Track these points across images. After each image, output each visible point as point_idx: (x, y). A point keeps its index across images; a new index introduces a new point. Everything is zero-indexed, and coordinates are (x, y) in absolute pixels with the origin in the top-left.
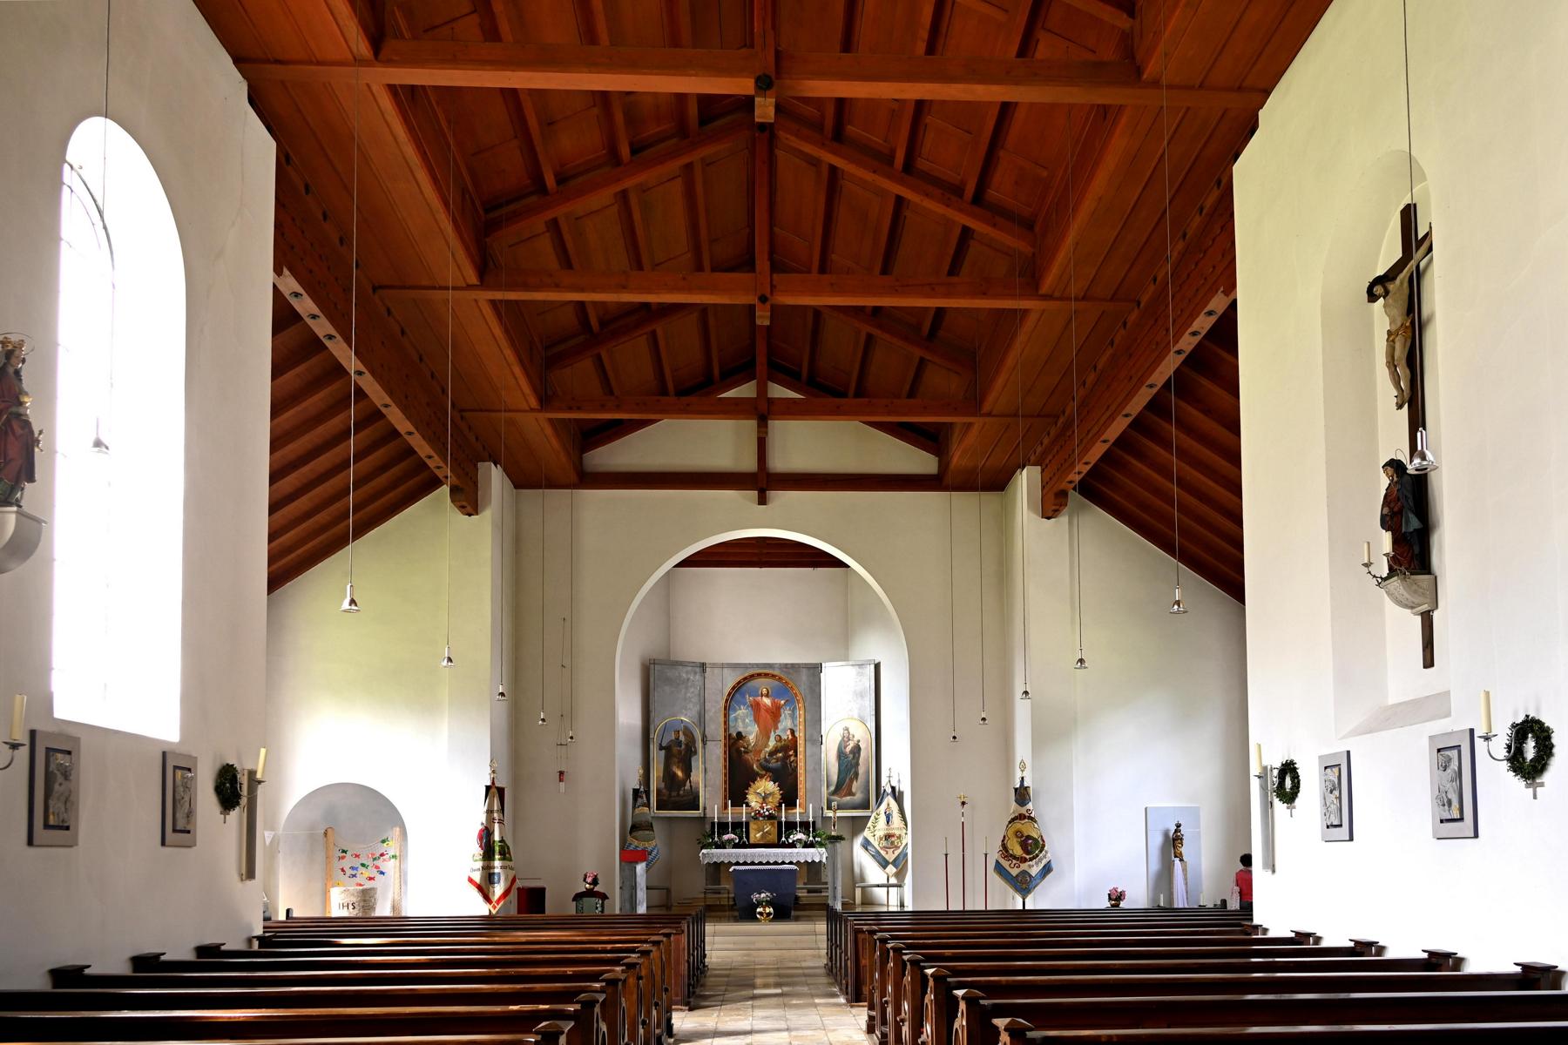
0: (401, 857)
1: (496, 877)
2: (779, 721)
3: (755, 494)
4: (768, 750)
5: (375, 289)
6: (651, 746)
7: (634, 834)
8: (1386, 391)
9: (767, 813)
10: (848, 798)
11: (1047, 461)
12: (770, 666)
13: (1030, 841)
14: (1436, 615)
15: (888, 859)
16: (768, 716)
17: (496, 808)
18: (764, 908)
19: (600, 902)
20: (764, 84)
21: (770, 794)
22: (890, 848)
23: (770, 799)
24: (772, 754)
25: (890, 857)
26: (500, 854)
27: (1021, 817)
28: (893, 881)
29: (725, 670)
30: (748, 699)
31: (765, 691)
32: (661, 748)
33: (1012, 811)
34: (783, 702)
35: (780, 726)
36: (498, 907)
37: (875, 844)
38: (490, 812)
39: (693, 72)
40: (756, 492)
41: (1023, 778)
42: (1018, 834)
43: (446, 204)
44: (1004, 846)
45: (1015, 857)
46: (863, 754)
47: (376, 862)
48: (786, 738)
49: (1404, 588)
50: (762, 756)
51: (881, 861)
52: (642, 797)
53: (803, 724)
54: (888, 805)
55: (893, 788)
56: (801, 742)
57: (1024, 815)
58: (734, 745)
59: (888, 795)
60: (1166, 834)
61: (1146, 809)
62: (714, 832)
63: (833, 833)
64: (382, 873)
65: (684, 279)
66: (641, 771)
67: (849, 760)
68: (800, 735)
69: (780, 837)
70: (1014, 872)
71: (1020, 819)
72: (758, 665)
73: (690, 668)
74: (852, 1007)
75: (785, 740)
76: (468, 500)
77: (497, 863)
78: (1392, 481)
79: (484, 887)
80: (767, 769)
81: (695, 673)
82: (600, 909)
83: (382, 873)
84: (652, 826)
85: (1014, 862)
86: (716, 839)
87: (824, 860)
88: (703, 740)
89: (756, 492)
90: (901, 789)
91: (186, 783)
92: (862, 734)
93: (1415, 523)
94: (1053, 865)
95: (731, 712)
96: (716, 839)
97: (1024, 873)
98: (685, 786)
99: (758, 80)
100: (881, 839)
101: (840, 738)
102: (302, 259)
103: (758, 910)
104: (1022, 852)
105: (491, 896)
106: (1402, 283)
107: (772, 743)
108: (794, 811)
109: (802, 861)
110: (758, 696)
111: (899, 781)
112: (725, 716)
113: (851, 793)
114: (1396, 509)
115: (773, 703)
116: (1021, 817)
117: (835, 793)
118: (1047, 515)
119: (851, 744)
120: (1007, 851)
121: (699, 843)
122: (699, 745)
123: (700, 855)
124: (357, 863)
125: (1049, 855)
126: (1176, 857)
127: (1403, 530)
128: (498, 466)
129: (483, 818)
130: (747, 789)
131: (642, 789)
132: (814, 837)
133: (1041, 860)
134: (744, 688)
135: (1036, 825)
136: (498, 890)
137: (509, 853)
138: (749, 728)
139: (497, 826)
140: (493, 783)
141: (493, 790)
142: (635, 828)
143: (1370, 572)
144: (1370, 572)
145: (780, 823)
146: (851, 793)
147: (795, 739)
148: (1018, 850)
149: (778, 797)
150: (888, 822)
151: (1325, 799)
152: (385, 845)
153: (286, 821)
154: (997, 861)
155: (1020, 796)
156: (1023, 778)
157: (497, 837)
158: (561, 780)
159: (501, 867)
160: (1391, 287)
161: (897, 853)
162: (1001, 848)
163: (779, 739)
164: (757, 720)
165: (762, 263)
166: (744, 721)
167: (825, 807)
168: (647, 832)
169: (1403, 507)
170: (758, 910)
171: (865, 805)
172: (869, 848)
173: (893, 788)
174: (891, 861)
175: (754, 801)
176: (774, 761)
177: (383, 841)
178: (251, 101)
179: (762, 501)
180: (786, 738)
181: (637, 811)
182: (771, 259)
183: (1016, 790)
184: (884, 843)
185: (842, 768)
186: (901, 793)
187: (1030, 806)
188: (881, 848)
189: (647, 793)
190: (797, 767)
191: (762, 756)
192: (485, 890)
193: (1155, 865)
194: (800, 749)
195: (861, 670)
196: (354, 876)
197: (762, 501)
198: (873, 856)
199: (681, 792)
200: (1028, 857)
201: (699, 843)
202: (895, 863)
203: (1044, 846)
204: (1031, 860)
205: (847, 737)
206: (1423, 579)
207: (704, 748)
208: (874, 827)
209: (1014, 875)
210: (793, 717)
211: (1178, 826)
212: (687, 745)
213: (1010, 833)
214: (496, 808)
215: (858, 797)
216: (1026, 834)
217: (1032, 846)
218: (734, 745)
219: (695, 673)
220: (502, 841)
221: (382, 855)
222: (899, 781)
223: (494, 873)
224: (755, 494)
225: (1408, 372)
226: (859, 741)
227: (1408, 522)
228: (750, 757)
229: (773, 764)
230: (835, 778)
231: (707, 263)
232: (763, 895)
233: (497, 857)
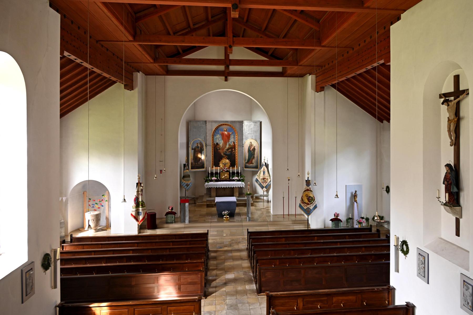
0: (109, 201)
1: (140, 213)
2: (230, 139)
3: (224, 77)
4: (226, 148)
5: (97, 42)
6: (189, 149)
7: (184, 179)
8: (446, 139)
9: (226, 170)
10: (251, 165)
11: (318, 75)
12: (227, 122)
13: (310, 198)
14: (461, 220)
15: (264, 186)
16: (226, 138)
17: (140, 190)
18: (226, 216)
19: (174, 216)
20: (235, 7)
21: (227, 163)
22: (264, 182)
23: (227, 165)
24: (227, 150)
25: (264, 185)
26: (141, 205)
27: (308, 190)
28: (265, 193)
29: (213, 123)
30: (220, 132)
31: (225, 129)
32: (192, 149)
33: (305, 188)
34: (231, 133)
35: (230, 141)
36: (141, 223)
37: (260, 181)
38: (138, 192)
39: (210, 1)
40: (224, 77)
41: (308, 177)
42: (307, 196)
43: (122, 24)
44: (302, 199)
45: (305, 203)
46: (256, 151)
47: (100, 202)
48: (232, 145)
49: (451, 211)
50: (224, 150)
51: (262, 186)
52: (186, 167)
53: (237, 140)
54: (264, 168)
55: (265, 163)
56: (236, 146)
57: (309, 190)
58: (216, 147)
59: (264, 165)
60: (352, 194)
61: (346, 185)
62: (209, 176)
63: (248, 193)
64: (103, 206)
65: (204, 39)
66: (186, 158)
67: (252, 152)
68: (236, 144)
69: (230, 177)
70: (305, 208)
71: (307, 191)
72: (223, 121)
73: (201, 123)
74: (259, 295)
75: (231, 145)
76: (130, 86)
77: (140, 209)
78: (448, 171)
79: (136, 216)
80: (226, 155)
81: (203, 124)
82: (174, 218)
83: (103, 206)
84: (190, 176)
85: (305, 204)
86: (210, 178)
87: (244, 187)
88: (206, 146)
89: (224, 77)
90: (268, 163)
91: (30, 276)
92: (255, 144)
93: (455, 190)
94: (317, 205)
95: (214, 136)
96: (210, 178)
97: (308, 208)
98: (200, 161)
99: (233, 5)
100: (262, 179)
101: (249, 145)
102: (71, 44)
103: (224, 217)
104: (308, 202)
105: (138, 219)
106: (454, 104)
107: (227, 146)
108: (234, 168)
109: (237, 187)
110: (223, 131)
111: (267, 161)
112: (213, 138)
113: (252, 163)
114: (449, 183)
115: (228, 133)
116: (308, 190)
117: (247, 163)
118: (317, 91)
119: (252, 147)
120: (303, 201)
121: (204, 180)
122: (205, 147)
123: (205, 185)
124: (94, 203)
125: (316, 202)
126: (355, 201)
127: (452, 191)
128: (140, 72)
129: (136, 194)
130: (220, 162)
131: (186, 164)
132: (241, 178)
133: (314, 204)
134: (219, 128)
135: (312, 193)
136: (141, 217)
137: (144, 204)
138: (220, 141)
139: (140, 196)
140: (139, 182)
141: (139, 184)
142: (184, 177)
143: (439, 200)
144: (439, 200)
145: (230, 173)
146: (252, 163)
147: (235, 145)
148: (306, 201)
149: (229, 164)
150: (264, 174)
151: (419, 265)
152: (103, 197)
153: (71, 191)
154: (300, 204)
155: (307, 183)
156: (308, 177)
157: (140, 200)
158: (161, 173)
159: (142, 210)
160: (450, 104)
161: (267, 184)
162: (301, 200)
163: (230, 145)
164: (223, 139)
165: (230, 34)
166: (218, 139)
167: (244, 167)
168: (188, 178)
169: (452, 182)
170: (224, 217)
171: (256, 167)
172: (258, 182)
173: (265, 163)
174: (264, 186)
175: (221, 165)
176: (228, 152)
177: (103, 196)
178: (51, 6)
179: (226, 80)
180: (232, 145)
181: (185, 171)
182: (233, 33)
183: (306, 181)
184: (262, 181)
185: (250, 155)
186: (268, 165)
187: (310, 187)
188: (262, 182)
189: (188, 165)
190: (235, 154)
191: (224, 150)
192: (137, 218)
193: (348, 204)
194: (236, 148)
195: (255, 124)
196: (93, 207)
197: (226, 80)
198: (259, 184)
199: (199, 163)
200: (309, 203)
201: (204, 180)
202: (266, 187)
203: (314, 199)
204: (310, 204)
205: (251, 145)
206: (458, 208)
207: (206, 148)
208: (259, 175)
209: (305, 209)
210: (234, 138)
211: (356, 191)
212: (201, 148)
213: (304, 195)
214: (140, 190)
215: (254, 164)
216: (309, 196)
217: (311, 200)
218: (216, 147)
219: (203, 124)
220: (142, 201)
221: (102, 200)
222: (267, 161)
223: (139, 212)
224: (224, 77)
225: (455, 135)
226: (255, 147)
227: (453, 188)
228: (220, 151)
229: (228, 153)
230: (247, 158)
231: (211, 34)
232: (226, 212)
233: (140, 206)
